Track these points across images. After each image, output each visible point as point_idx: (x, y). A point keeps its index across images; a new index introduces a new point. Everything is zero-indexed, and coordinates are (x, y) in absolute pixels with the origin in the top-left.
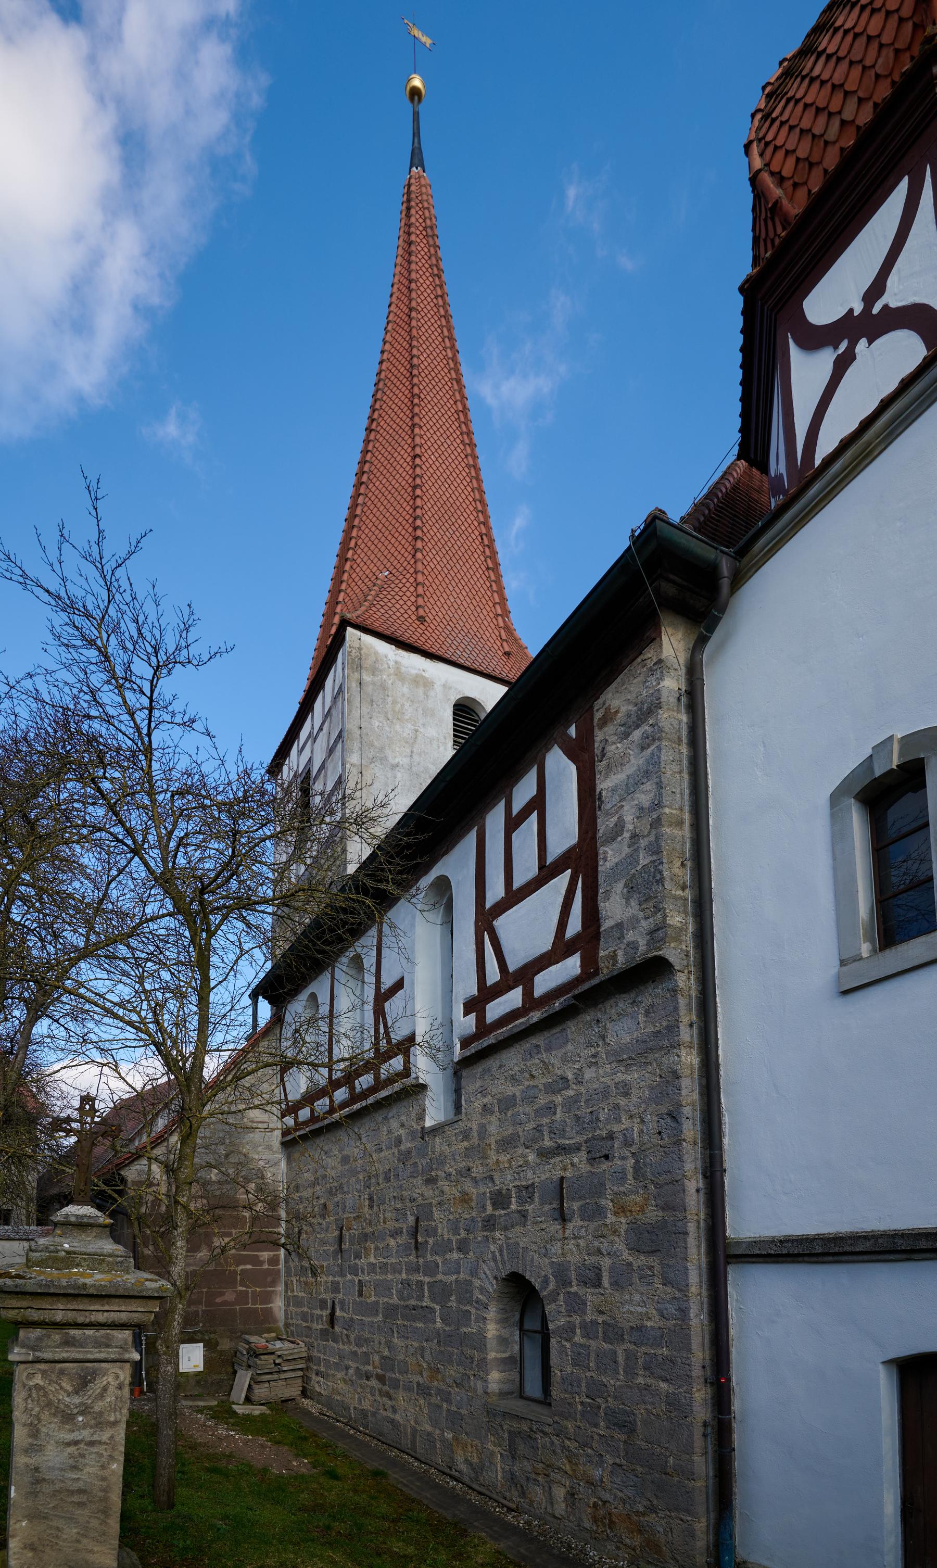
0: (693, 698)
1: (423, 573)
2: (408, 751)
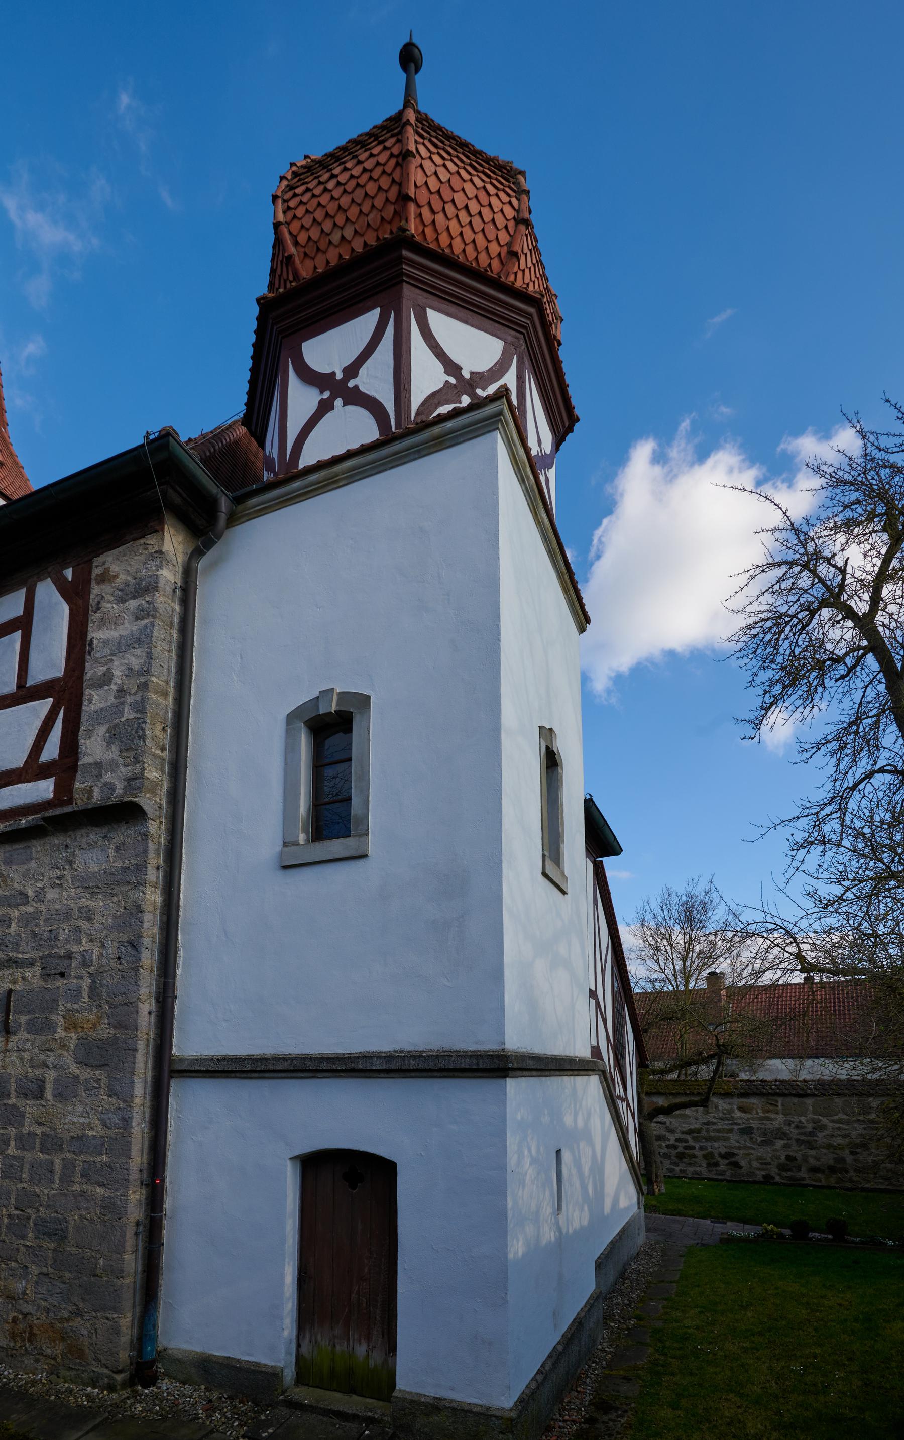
0: (186, 594)
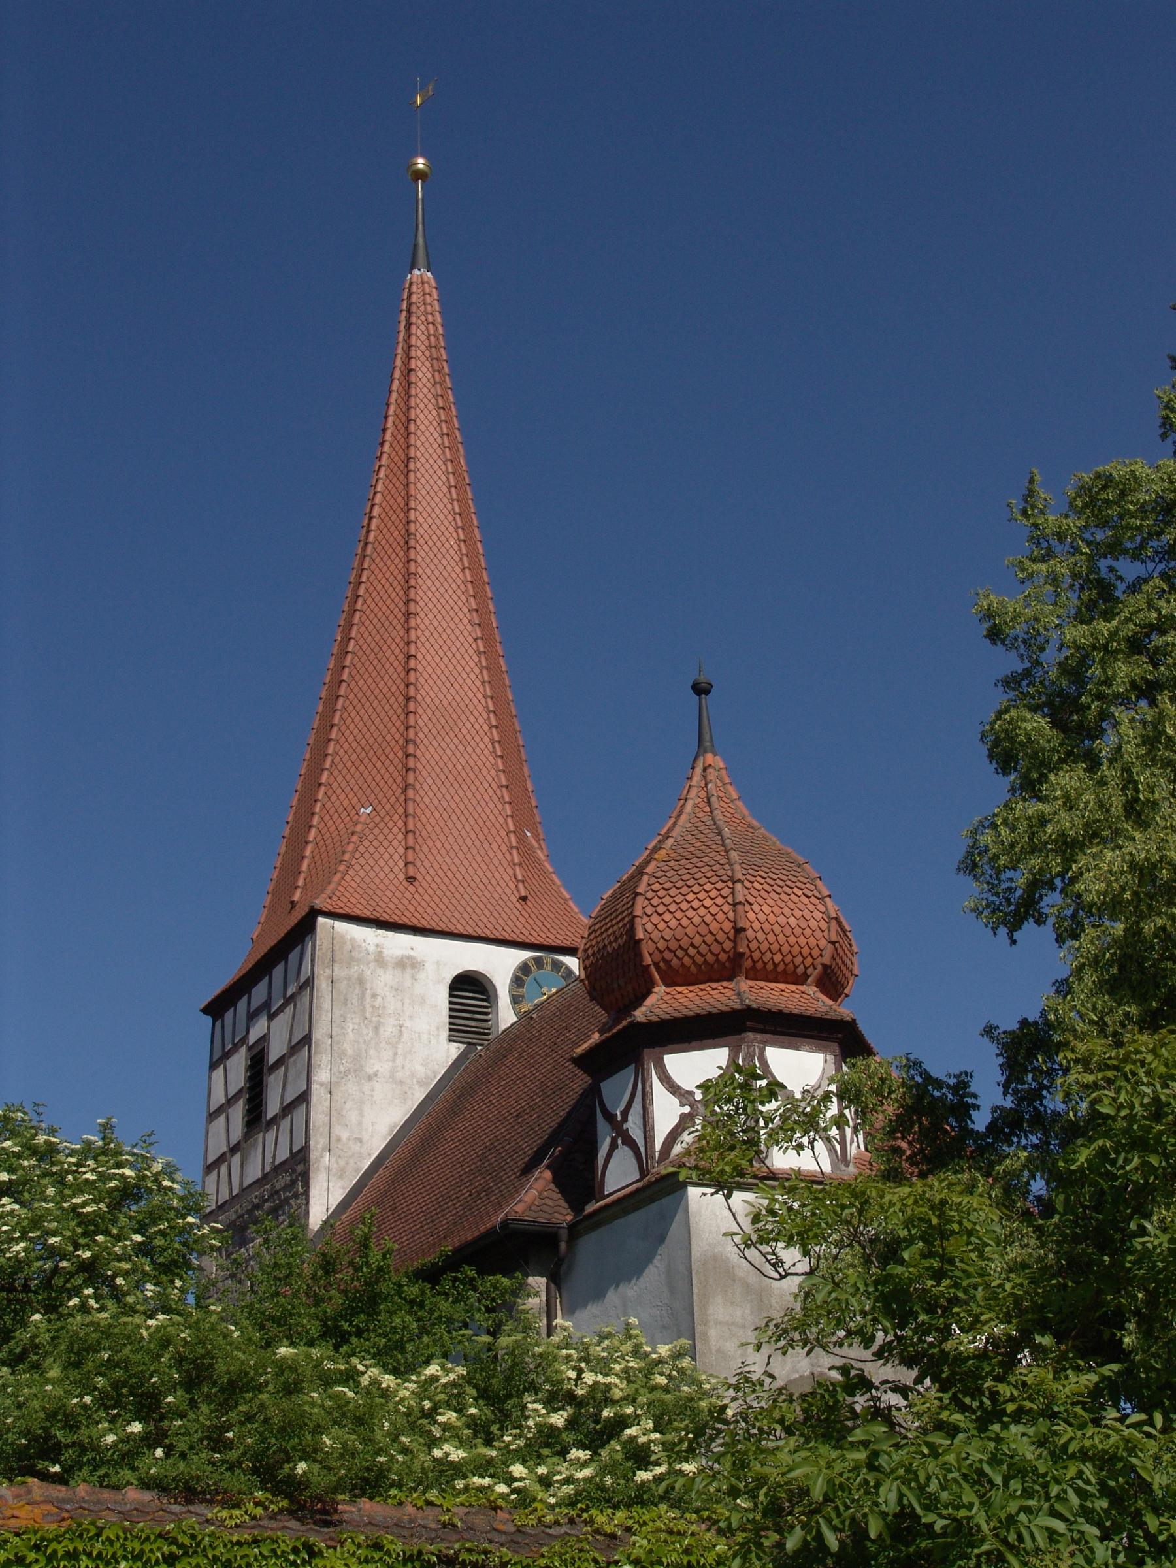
1: (415, 801)
2: (391, 1053)
